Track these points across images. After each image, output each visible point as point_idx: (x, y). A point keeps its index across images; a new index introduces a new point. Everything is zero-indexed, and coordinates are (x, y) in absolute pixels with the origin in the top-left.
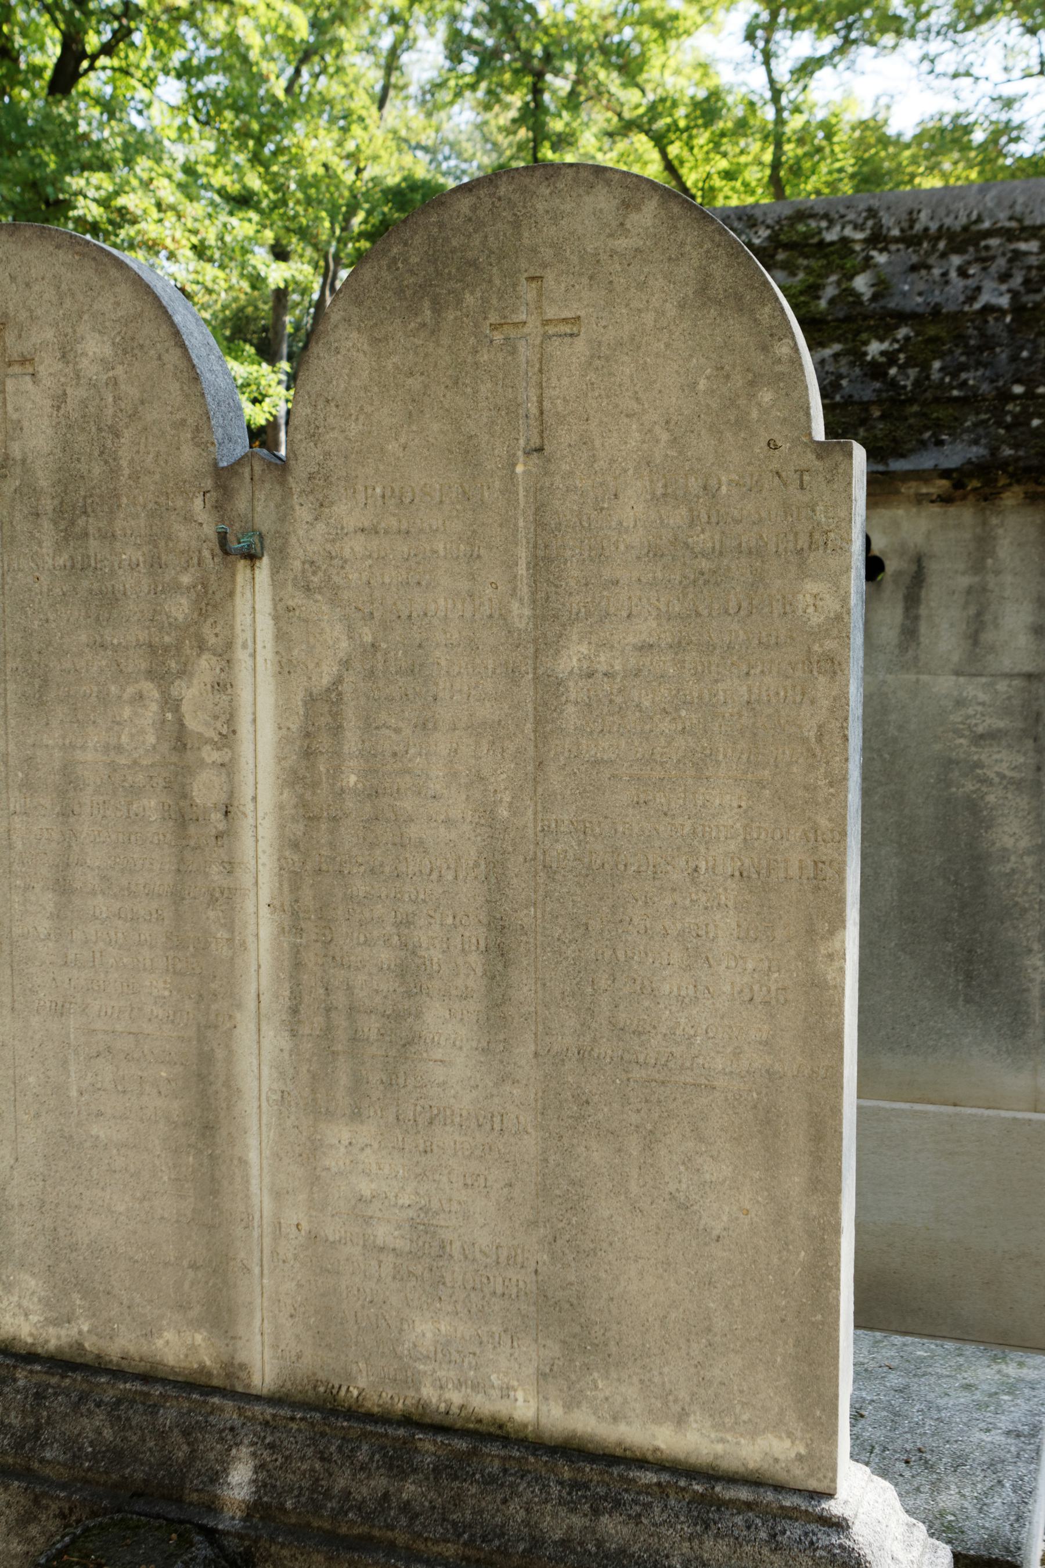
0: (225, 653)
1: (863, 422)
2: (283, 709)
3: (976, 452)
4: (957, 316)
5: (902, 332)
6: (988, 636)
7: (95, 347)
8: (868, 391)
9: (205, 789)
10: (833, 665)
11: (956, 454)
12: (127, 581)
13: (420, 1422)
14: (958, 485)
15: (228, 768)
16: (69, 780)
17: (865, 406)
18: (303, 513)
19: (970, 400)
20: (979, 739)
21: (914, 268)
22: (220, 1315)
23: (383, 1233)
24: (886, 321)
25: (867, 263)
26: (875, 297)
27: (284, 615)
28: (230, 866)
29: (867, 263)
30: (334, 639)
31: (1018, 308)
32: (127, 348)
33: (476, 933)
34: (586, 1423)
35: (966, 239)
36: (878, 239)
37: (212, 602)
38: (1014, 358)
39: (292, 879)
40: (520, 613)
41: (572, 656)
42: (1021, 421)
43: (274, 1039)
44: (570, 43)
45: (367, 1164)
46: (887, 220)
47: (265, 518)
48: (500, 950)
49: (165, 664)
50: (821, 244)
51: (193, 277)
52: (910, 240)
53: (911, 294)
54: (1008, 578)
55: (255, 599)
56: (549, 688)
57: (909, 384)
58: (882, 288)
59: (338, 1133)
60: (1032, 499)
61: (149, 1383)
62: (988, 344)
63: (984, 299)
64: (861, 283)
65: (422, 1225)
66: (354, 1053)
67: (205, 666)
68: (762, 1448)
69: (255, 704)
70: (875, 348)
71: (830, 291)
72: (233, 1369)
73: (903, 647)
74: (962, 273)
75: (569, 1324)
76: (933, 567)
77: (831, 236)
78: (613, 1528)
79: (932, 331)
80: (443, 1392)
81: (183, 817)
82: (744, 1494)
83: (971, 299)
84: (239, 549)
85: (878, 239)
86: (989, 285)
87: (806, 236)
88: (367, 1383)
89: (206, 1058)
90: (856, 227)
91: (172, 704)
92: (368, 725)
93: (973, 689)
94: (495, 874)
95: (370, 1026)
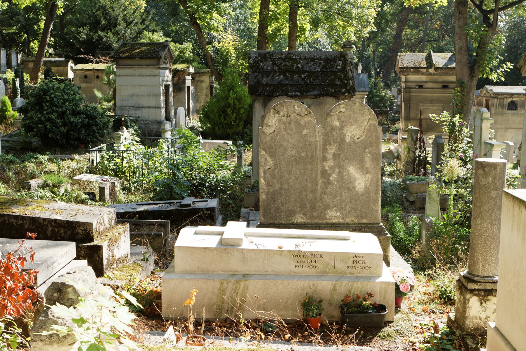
3: (319, 92)
4: (313, 72)
5: (306, 74)
8: (303, 83)
11: (316, 92)
19: (317, 85)
24: (304, 72)
25: (300, 62)
29: (300, 62)
31: (321, 71)
35: (313, 60)
42: (323, 88)
44: (503, 45)
46: (302, 56)
52: (305, 59)
53: (307, 68)
62: (318, 76)
64: (299, 65)
69: (147, 76)
70: (303, 76)
71: (295, 67)
77: (294, 57)
82: (342, 225)
85: (301, 59)
86: (317, 67)
87: (291, 57)
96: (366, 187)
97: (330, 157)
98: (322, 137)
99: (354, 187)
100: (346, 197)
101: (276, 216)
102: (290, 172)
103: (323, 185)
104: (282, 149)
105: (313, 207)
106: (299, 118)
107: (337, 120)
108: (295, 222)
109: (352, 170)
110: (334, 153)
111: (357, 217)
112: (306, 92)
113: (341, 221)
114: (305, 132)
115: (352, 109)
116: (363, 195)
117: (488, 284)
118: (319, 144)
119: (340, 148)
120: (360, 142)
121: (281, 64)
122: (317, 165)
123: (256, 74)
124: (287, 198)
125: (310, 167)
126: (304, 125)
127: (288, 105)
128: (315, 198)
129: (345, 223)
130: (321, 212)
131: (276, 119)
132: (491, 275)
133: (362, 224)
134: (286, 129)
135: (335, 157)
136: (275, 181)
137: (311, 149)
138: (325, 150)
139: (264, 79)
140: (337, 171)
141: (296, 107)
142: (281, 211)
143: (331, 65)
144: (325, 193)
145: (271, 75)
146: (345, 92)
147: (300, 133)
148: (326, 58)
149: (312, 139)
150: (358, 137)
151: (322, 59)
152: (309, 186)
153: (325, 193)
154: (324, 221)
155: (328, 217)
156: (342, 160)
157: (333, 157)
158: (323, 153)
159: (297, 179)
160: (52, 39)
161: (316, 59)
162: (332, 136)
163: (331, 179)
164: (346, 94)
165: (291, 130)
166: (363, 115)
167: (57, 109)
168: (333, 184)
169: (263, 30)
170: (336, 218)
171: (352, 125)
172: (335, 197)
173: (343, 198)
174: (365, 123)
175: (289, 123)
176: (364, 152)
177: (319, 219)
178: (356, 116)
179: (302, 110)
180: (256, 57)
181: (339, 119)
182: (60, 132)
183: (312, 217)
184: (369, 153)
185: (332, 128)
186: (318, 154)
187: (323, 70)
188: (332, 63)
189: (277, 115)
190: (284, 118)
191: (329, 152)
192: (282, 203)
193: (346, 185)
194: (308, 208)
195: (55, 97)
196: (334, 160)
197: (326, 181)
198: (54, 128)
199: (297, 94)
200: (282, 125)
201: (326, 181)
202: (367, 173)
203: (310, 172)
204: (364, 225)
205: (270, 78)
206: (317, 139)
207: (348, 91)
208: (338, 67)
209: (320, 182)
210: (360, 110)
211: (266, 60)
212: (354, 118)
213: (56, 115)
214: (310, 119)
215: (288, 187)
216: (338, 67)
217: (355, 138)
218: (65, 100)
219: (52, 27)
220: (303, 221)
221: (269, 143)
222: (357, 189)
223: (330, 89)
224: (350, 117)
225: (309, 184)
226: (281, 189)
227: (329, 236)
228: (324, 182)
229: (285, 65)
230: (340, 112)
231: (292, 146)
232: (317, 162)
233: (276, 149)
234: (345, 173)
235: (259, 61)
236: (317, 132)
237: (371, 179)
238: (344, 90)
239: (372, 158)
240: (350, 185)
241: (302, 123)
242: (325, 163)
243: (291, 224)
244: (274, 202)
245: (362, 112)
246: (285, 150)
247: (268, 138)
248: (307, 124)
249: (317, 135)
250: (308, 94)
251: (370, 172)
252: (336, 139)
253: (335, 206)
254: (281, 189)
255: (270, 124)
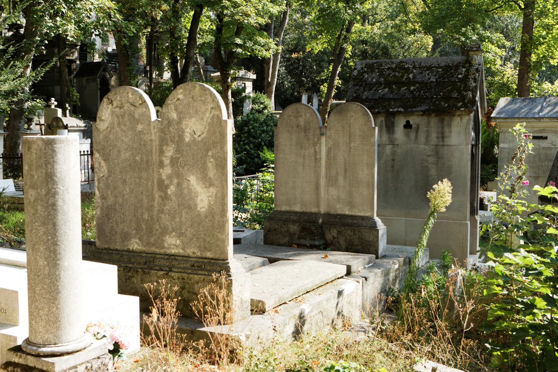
0: (320, 144)
1: (409, 101)
2: (326, 149)
3: (427, 107)
4: (426, 83)
5: (417, 85)
6: (429, 139)
7: (308, 115)
9: (318, 157)
10: (374, 146)
11: (423, 108)
12: (311, 137)
13: (338, 215)
14: (424, 113)
15: (320, 155)
16: (304, 156)
17: (410, 99)
18: (328, 131)
20: (428, 156)
21: (420, 73)
22: (318, 206)
23: (334, 197)
26: (413, 79)
27: (326, 141)
28: (320, 164)
30: (331, 143)
31: (436, 81)
32: (311, 115)
33: (343, 169)
34: (353, 213)
35: (429, 68)
36: (414, 67)
37: (319, 139)
38: (435, 91)
39: (326, 165)
40: (348, 141)
41: (352, 145)
43: (324, 180)
45: (333, 191)
47: (324, 131)
48: (346, 171)
49: (314, 145)
50: (405, 68)
51: (256, 21)
52: (420, 68)
53: (419, 78)
54: (433, 129)
55: (323, 139)
56: (350, 148)
57: (417, 95)
58: (414, 77)
59: (330, 188)
60: (436, 115)
61: (311, 214)
63: (431, 80)
65: (338, 197)
66: (332, 181)
67: (318, 145)
68: (368, 214)
70: (412, 88)
71: (405, 77)
72: (319, 212)
73: (415, 140)
74: (428, 75)
75: (351, 204)
76: (420, 126)
77: (406, 66)
78: (355, 221)
79: (422, 85)
80: (340, 212)
81: (316, 159)
82: (181, 258)
83: (429, 80)
84: (322, 134)
85: (414, 67)
86: (432, 77)
88: (332, 212)
89: (318, 182)
90: (411, 65)
91: (315, 149)
92: (334, 151)
93: (427, 147)
94: (345, 165)
95: (333, 178)
96: (210, 206)
97: (167, 161)
98: (158, 134)
99: (196, 205)
100: (186, 218)
101: (111, 239)
102: (124, 182)
103: (160, 201)
104: (115, 151)
105: (150, 230)
106: (132, 108)
107: (174, 111)
108: (131, 248)
109: (193, 180)
110: (172, 156)
111: (199, 247)
112: (411, 108)
113: (181, 251)
114: (140, 127)
115: (191, 95)
116: (206, 217)
117: (29, 357)
118: (154, 144)
119: (178, 150)
120: (202, 141)
121: (390, 74)
122: (153, 173)
123: (357, 87)
124: (122, 216)
125: (145, 175)
126: (138, 118)
127: (121, 92)
128: (152, 217)
129: (186, 255)
130: (158, 238)
131: (109, 111)
132: (40, 341)
133: (206, 258)
134: (119, 124)
135: (174, 162)
136: (109, 193)
137: (147, 151)
138: (162, 152)
139: (366, 93)
140: (175, 181)
141: (130, 94)
142: (116, 233)
143: (451, 73)
144: (162, 211)
145: (374, 89)
146: (461, 107)
147: (133, 129)
148: (446, 66)
149: (147, 138)
150: (199, 134)
151: (440, 67)
152: (145, 201)
153: (162, 211)
154: (162, 251)
155: (166, 245)
156: (181, 166)
157: (170, 162)
158: (159, 156)
159: (132, 191)
160: (340, 82)
161: (433, 67)
162: (169, 132)
163: (169, 193)
164: (462, 109)
165: (125, 125)
166: (204, 102)
167: (254, 140)
168: (171, 200)
169: (525, 57)
170: (175, 247)
171: (191, 118)
172: (173, 218)
173: (183, 220)
174: (208, 115)
175: (123, 116)
176: (207, 155)
177: (157, 247)
178: (195, 104)
179: (136, 98)
180: (362, 68)
181: (176, 109)
182: (254, 163)
183: (148, 244)
184: (213, 156)
185: (169, 122)
186: (154, 158)
187: (439, 80)
188: (452, 71)
189: (110, 106)
190: (118, 109)
191: (166, 155)
192: (116, 223)
193: (186, 202)
194: (144, 231)
195: (253, 128)
196: (172, 167)
197: (163, 195)
198: (249, 159)
199: (399, 110)
200: (116, 119)
201: (163, 195)
202: (210, 185)
203: (145, 182)
204: (206, 261)
205: (372, 92)
206: (153, 137)
207: (465, 105)
208: (460, 76)
209: (157, 196)
210: (200, 96)
211: (373, 71)
212: (193, 107)
213: (252, 146)
214: (144, 110)
215: (123, 202)
216: (460, 76)
217: (196, 136)
218: (263, 131)
219: (339, 69)
220: (139, 248)
221: (102, 143)
222: (199, 209)
223: (443, 103)
224: (190, 106)
225: (145, 198)
226: (115, 204)
227: (9, 260)
228: (160, 196)
229: (394, 76)
230: (178, 99)
231: (126, 146)
232: (153, 169)
233: (110, 151)
234: (185, 185)
235: (365, 72)
236: (152, 128)
237: (216, 195)
238: (460, 104)
239: (217, 165)
240: (191, 203)
241: (136, 116)
242: (161, 170)
243: (126, 251)
244: (108, 220)
245: (203, 98)
246: (119, 151)
247: (102, 136)
248: (142, 117)
249: (153, 132)
250: (414, 109)
251: (214, 185)
252: (174, 137)
253: (173, 231)
254: (115, 204)
255: (103, 118)
